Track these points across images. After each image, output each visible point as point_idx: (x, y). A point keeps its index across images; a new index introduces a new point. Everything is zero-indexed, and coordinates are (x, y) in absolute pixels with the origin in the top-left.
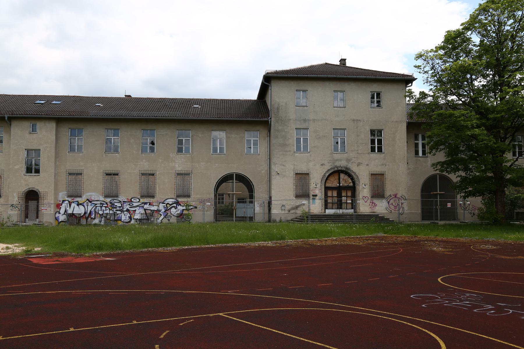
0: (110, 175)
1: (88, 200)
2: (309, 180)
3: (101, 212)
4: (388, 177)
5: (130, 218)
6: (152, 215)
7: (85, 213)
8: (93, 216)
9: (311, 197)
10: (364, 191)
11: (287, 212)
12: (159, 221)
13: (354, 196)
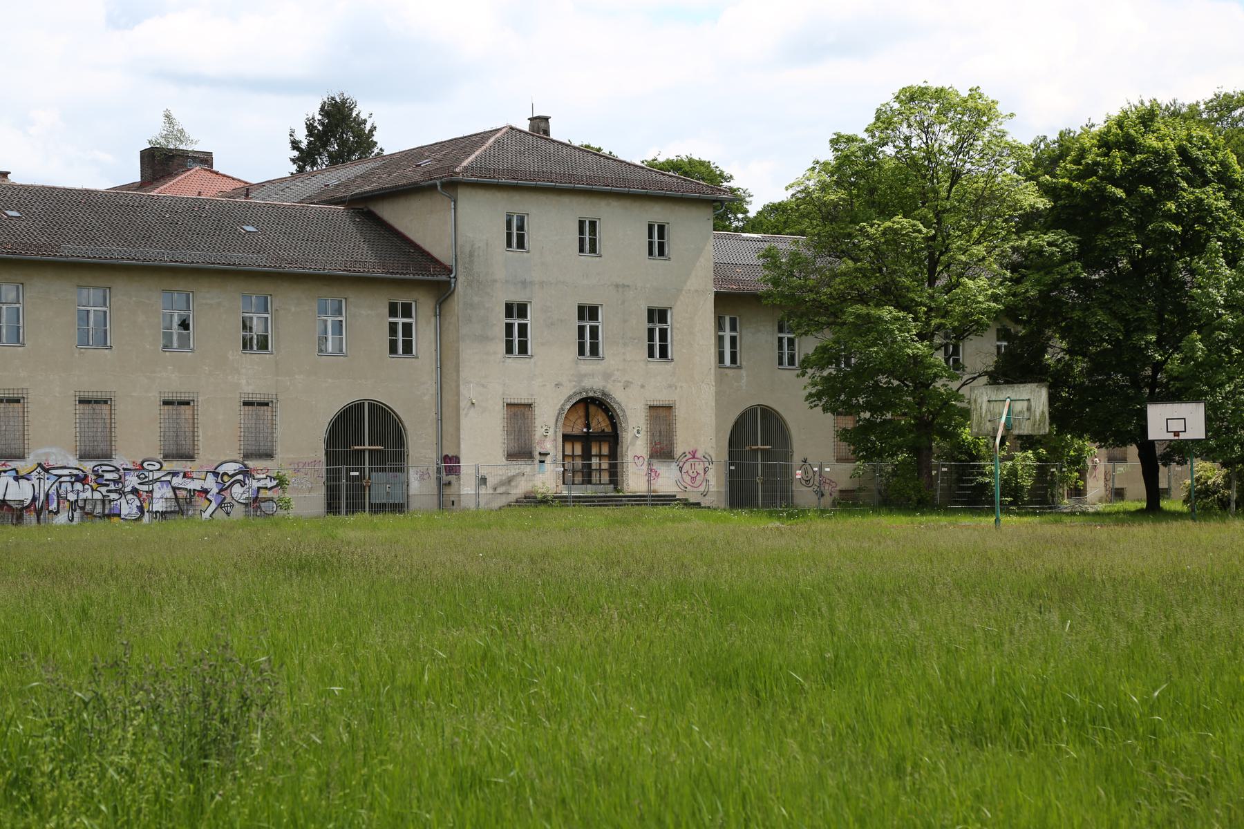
0: (89, 402)
1: (39, 465)
2: (532, 419)
3: (72, 497)
4: (680, 413)
5: (141, 509)
6: (189, 502)
7: (34, 499)
8: (53, 506)
9: (537, 457)
10: (635, 444)
11: (491, 491)
12: (206, 515)
13: (613, 455)
